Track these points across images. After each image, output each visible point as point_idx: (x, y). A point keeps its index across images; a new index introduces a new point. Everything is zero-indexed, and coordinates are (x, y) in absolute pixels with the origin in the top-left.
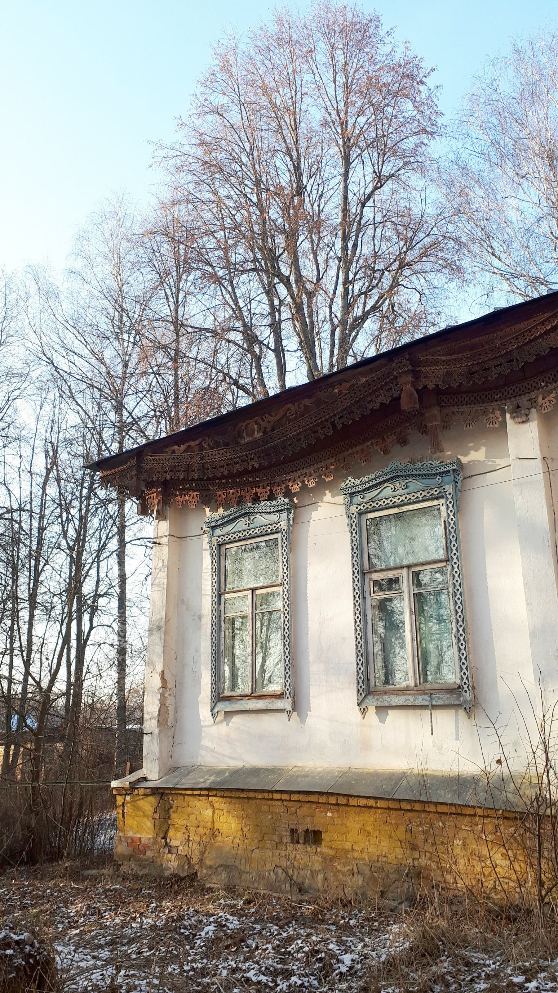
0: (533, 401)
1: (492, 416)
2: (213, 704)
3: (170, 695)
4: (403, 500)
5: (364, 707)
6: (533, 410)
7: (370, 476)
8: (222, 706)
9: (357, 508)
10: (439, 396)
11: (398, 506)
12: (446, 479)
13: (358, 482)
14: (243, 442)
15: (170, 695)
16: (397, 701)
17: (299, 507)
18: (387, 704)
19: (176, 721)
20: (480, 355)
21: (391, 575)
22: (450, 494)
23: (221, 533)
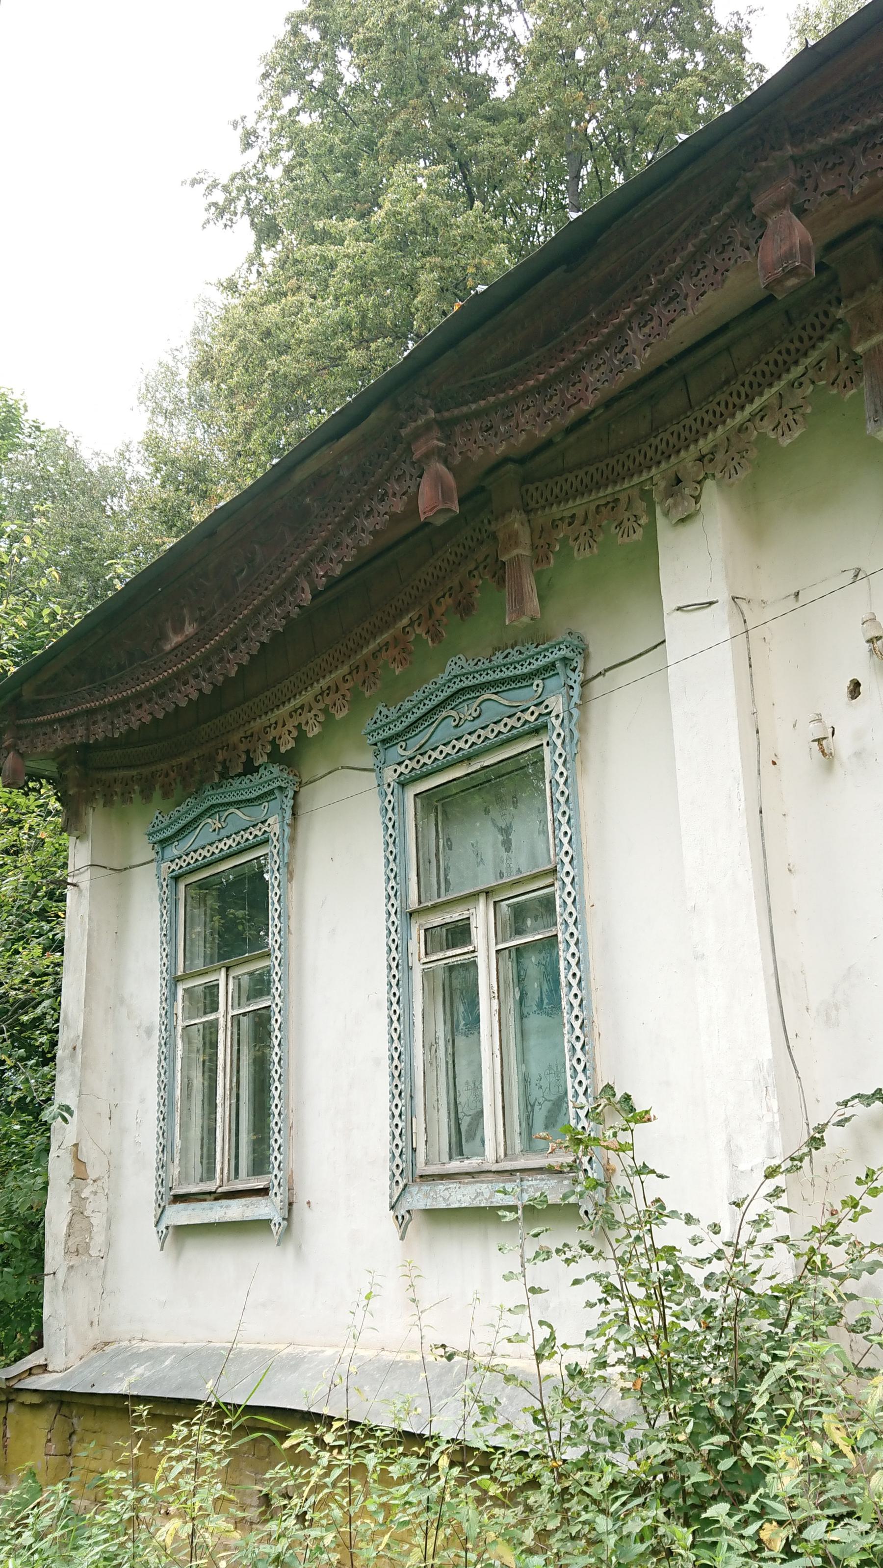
0: (706, 459)
1: (627, 514)
2: (160, 1210)
3: (95, 1193)
4: (473, 744)
5: (403, 1212)
6: (709, 484)
7: (413, 698)
8: (420, 1198)
9: (395, 771)
10: (524, 488)
11: (469, 758)
12: (552, 683)
13: (393, 713)
14: (168, 647)
15: (95, 1193)
16: (460, 1197)
17: (307, 784)
18: (443, 1205)
19: (109, 1244)
20: (562, 351)
21: (454, 915)
22: (557, 716)
23: (176, 852)
